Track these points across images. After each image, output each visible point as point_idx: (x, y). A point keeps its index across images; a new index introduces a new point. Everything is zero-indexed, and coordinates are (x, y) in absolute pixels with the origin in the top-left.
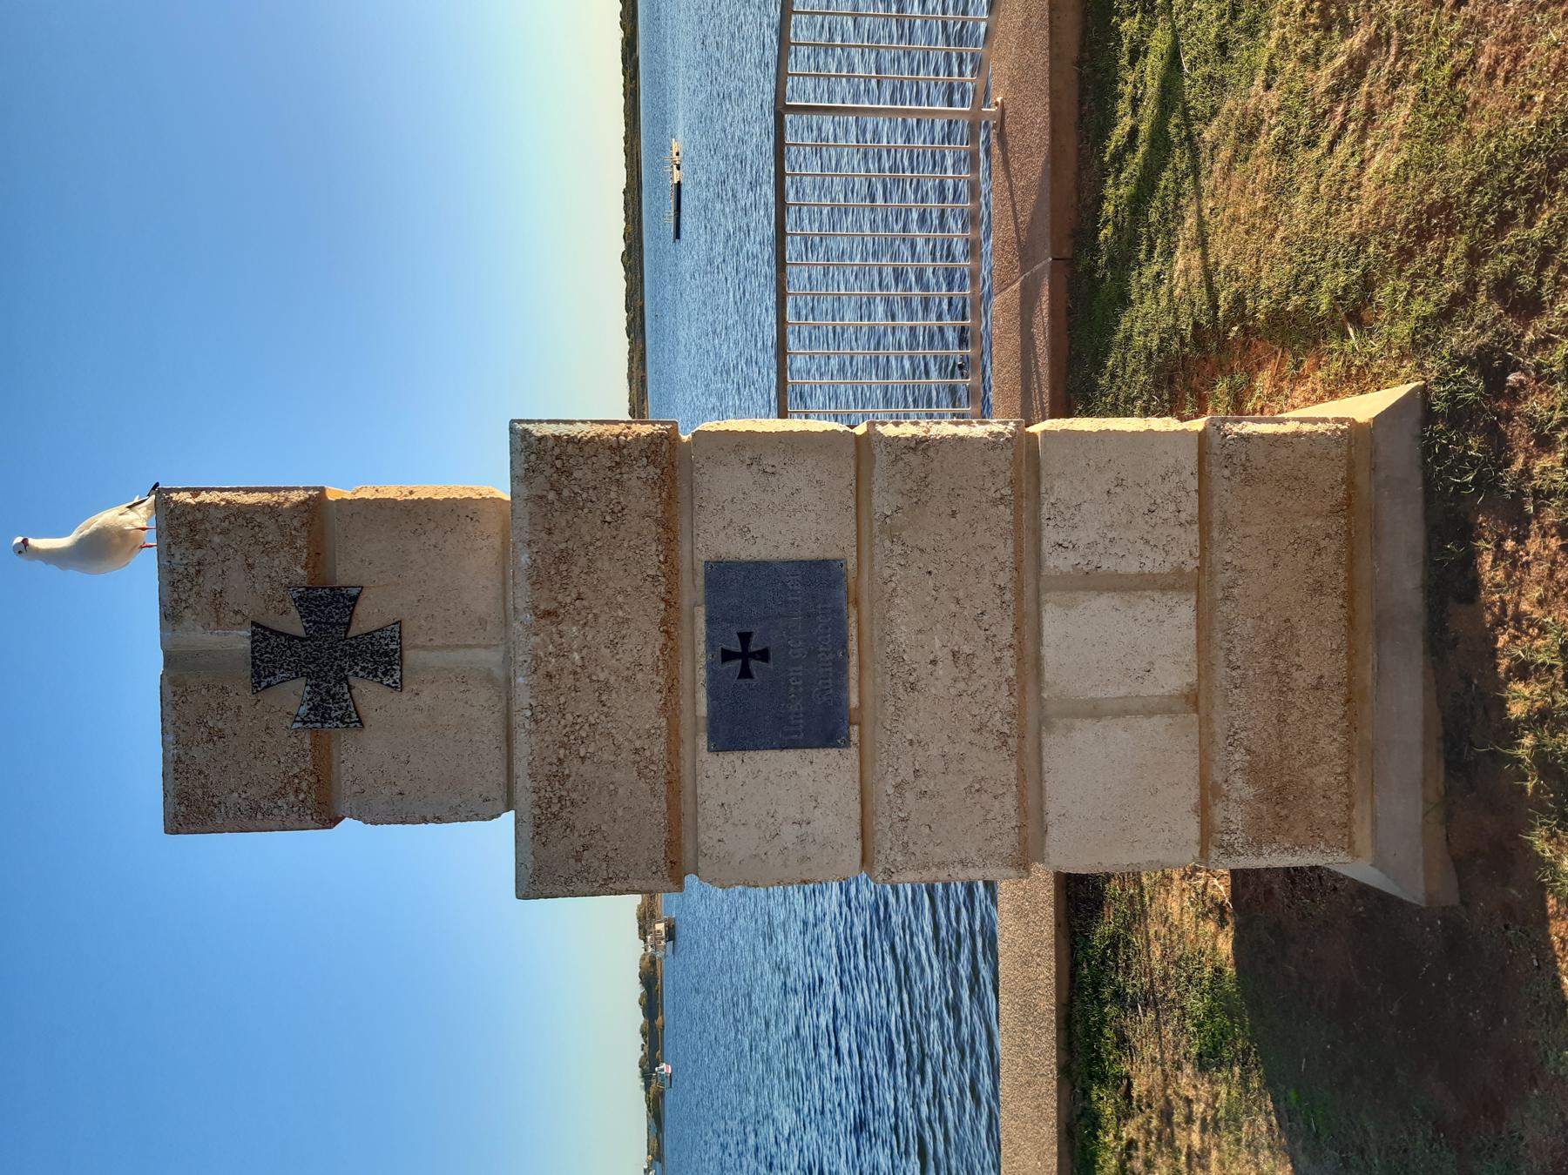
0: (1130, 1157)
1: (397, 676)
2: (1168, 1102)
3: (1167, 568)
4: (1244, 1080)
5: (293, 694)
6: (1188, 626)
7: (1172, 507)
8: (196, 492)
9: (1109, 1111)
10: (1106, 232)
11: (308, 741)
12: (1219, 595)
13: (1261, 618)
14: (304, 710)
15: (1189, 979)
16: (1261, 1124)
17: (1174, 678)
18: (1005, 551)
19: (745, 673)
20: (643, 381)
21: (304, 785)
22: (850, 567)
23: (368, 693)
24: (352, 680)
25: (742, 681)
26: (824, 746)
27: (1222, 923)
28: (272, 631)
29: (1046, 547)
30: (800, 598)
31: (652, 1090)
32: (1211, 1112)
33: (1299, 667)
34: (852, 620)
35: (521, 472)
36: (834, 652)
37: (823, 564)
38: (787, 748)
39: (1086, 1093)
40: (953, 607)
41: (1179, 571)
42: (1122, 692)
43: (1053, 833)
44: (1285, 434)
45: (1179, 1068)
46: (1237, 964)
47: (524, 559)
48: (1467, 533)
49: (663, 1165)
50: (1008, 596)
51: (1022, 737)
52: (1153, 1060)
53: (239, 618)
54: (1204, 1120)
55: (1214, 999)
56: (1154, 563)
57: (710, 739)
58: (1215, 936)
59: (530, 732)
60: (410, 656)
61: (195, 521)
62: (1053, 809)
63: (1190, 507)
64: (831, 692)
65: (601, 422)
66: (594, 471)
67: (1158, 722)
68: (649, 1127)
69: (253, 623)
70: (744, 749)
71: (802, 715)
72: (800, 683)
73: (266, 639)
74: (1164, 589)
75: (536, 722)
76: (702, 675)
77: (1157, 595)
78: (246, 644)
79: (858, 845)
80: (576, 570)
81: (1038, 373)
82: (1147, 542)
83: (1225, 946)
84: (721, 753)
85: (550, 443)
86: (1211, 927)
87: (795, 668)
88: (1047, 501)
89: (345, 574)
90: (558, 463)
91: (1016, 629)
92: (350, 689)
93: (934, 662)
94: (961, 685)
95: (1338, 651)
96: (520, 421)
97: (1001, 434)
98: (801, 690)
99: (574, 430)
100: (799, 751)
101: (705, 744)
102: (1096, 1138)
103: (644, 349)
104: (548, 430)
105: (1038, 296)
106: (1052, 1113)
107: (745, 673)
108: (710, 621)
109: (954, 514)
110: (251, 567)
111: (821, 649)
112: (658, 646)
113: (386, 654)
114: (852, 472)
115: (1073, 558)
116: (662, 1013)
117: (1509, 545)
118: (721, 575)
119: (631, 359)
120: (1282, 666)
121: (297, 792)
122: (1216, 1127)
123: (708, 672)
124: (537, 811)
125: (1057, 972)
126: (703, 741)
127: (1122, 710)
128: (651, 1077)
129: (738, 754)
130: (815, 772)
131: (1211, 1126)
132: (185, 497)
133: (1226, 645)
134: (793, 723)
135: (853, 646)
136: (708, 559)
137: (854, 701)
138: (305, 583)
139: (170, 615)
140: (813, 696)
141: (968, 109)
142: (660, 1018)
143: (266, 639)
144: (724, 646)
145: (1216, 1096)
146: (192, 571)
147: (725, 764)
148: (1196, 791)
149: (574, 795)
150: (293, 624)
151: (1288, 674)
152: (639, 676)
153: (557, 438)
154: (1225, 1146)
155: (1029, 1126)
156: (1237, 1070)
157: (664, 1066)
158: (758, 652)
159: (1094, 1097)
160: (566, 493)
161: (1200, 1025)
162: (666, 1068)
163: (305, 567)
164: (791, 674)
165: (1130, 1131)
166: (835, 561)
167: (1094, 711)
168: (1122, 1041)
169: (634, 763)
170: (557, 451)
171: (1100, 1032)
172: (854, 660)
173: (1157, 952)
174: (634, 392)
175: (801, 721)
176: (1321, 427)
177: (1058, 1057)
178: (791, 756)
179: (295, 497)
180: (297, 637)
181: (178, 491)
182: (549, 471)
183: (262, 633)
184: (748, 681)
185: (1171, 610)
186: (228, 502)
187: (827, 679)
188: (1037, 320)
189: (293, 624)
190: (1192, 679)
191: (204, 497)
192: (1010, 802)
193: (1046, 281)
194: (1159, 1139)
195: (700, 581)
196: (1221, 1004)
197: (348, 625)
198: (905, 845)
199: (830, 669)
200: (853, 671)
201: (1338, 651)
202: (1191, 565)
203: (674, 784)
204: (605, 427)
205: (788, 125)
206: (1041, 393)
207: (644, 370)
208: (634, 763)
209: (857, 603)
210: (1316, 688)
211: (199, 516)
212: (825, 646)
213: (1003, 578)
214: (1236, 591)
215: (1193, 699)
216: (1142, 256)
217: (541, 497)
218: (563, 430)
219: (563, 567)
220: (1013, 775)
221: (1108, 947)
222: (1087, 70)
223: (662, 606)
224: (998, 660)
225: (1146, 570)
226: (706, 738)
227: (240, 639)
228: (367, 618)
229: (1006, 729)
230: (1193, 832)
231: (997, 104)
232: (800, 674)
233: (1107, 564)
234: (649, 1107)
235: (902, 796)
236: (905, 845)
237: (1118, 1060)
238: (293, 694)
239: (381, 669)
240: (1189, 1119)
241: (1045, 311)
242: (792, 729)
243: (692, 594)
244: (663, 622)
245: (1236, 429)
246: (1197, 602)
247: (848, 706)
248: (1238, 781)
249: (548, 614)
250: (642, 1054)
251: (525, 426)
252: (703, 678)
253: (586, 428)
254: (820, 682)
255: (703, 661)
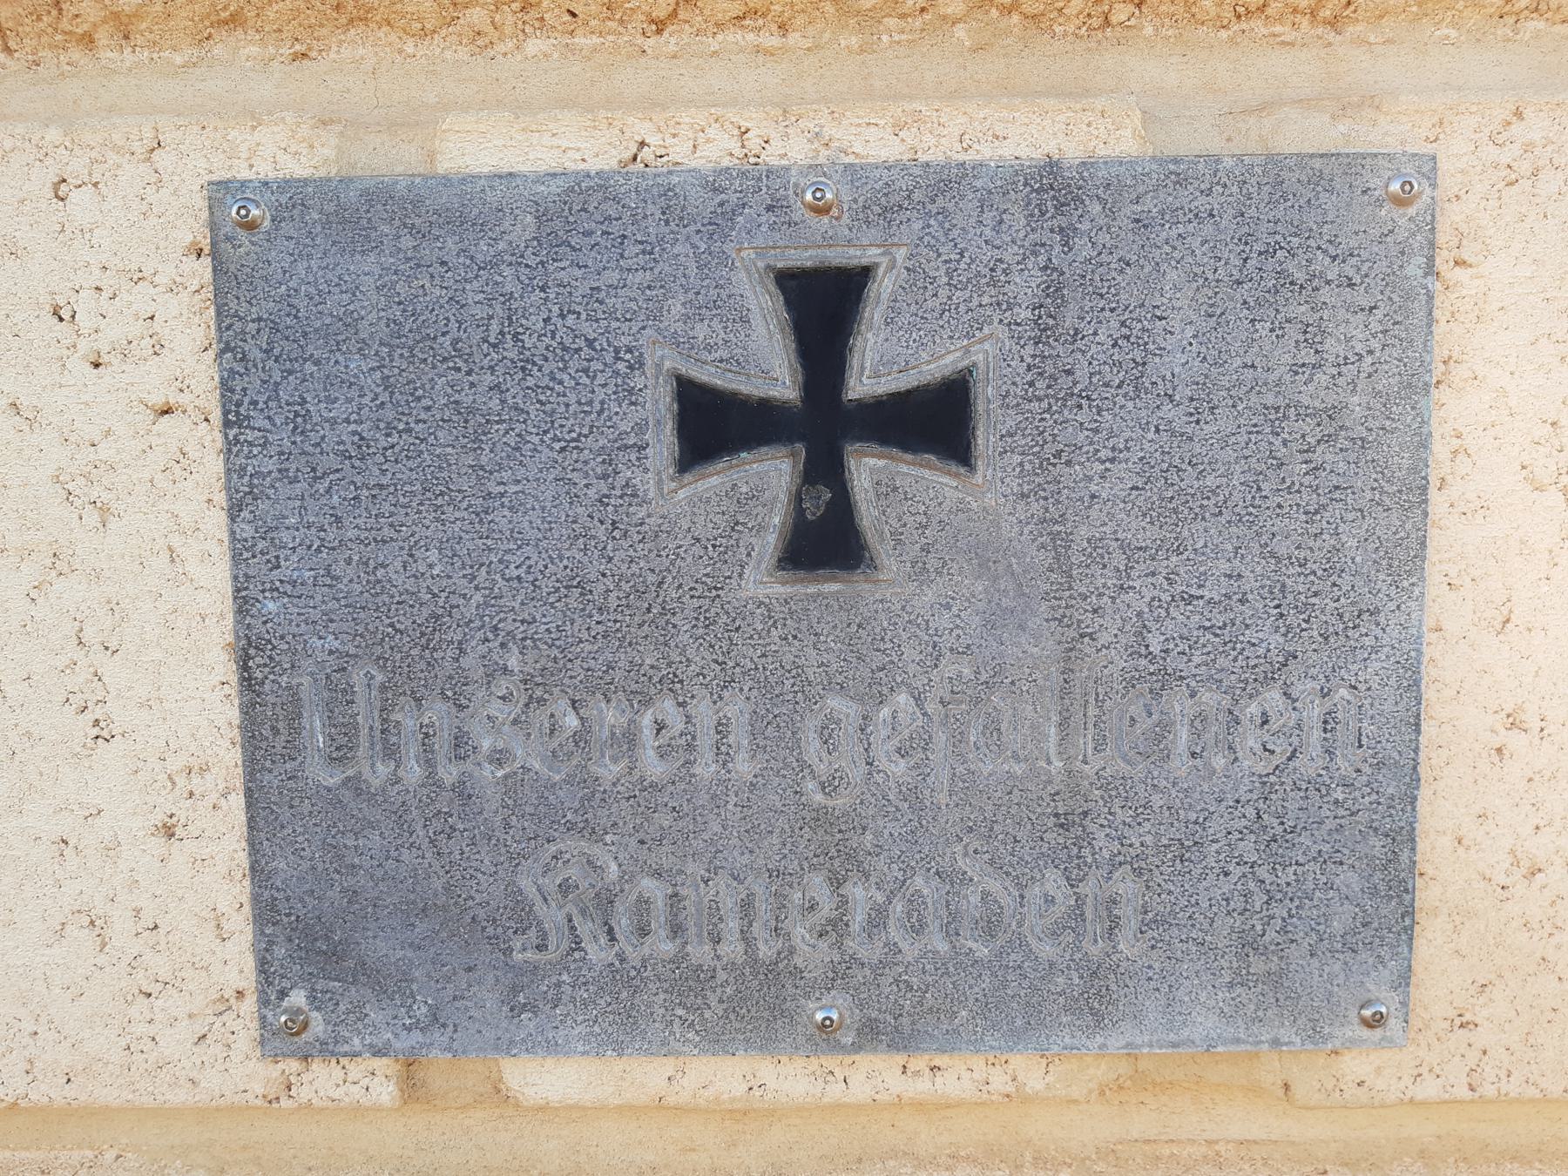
22: (1354, 1065)
25: (660, 404)
26: (266, 912)
30: (1180, 765)
36: (837, 976)
38: (248, 682)
64: (597, 953)
70: (232, 420)
71: (449, 773)
72: (653, 766)
84: (204, 268)
87: (739, 736)
98: (609, 770)
100: (229, 758)
101: (265, 170)
111: (857, 892)
123: (714, 183)
130: (111, 849)
134: (407, 720)
136: (1448, 181)
140: (571, 845)
144: (883, 287)
147: (139, 299)
158: (843, 506)
164: (704, 711)
166: (1404, 980)
175: (414, 772)
184: (663, 443)
187: (676, 930)
199: (732, 948)
205: (812, 589)
212: (877, 919)
222: (257, 566)
226: (298, 168)
232: (706, 769)
242: (364, 713)
247: (507, 1047)
252: (679, 152)
254: (648, 884)
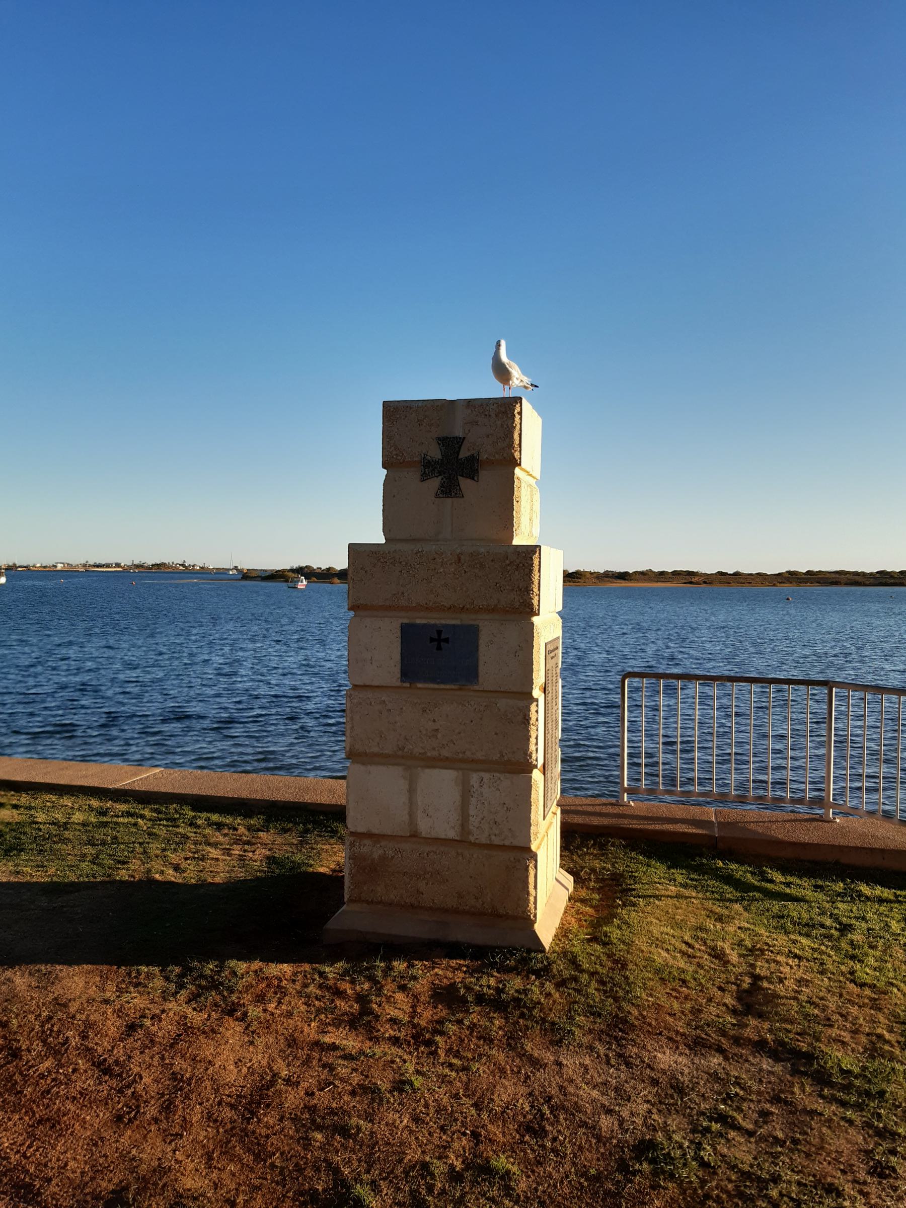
0: (230, 829)
1: (441, 495)
2: (254, 844)
3: (471, 827)
4: (260, 871)
5: (435, 453)
6: (446, 835)
7: (497, 832)
8: (520, 413)
9: (252, 822)
10: (720, 864)
11: (417, 459)
12: (459, 851)
13: (449, 868)
14: (429, 458)
15: (310, 856)
16: (241, 874)
17: (424, 826)
18: (480, 755)
19: (432, 640)
20: (836, 583)
21: (399, 458)
23: (435, 483)
24: (440, 478)
27: (334, 871)
28: (461, 445)
29: (482, 774)
31: (290, 574)
32: (248, 858)
33: (427, 884)
34: (453, 687)
35: (518, 550)
37: (476, 676)
39: (260, 813)
40: (457, 731)
41: (470, 833)
42: (419, 803)
43: (362, 768)
44: (528, 887)
45: (269, 850)
46: (313, 872)
47: (482, 550)
48: (473, 958)
49: (240, 580)
50: (461, 755)
51: (403, 757)
52: (275, 841)
53: (467, 432)
54: (245, 856)
55: (299, 864)
56: (474, 822)
57: (406, 624)
58: (328, 867)
59: (412, 551)
60: (449, 500)
61: (507, 414)
62: (373, 769)
63: (497, 841)
65: (539, 583)
66: (517, 580)
67: (406, 818)
68: (266, 571)
69: (464, 438)
73: (458, 443)
74: (462, 825)
75: (416, 553)
76: (432, 622)
77: (460, 822)
78: (457, 434)
79: (362, 684)
80: (477, 571)
81: (651, 824)
82: (483, 819)
83: (322, 870)
85: (530, 562)
86: (333, 866)
88: (502, 776)
89: (484, 474)
90: (521, 565)
91: (447, 758)
92: (437, 477)
93: (434, 721)
94: (424, 732)
95: (434, 903)
96: (540, 550)
97: (531, 757)
99: (536, 572)
102: (240, 816)
103: (865, 585)
104: (536, 562)
105: (702, 828)
106: (254, 796)
107: (432, 640)
108: (454, 626)
109: (496, 734)
110: (488, 436)
112: (445, 604)
113: (450, 491)
114: (515, 690)
115: (476, 785)
116: (342, 583)
117: (465, 969)
118: (473, 632)
119: (856, 574)
120: (428, 876)
121: (397, 455)
122: (241, 860)
124: (381, 553)
125: (323, 804)
126: (406, 621)
127: (411, 802)
128: (298, 573)
129: (400, 635)
131: (242, 858)
132: (517, 409)
133: (438, 852)
135: (442, 686)
137: (420, 685)
138: (480, 458)
139: (470, 403)
141: (831, 800)
142: (339, 581)
143: (458, 443)
145: (255, 861)
146: (487, 413)
148: (377, 832)
149: (387, 568)
150: (464, 454)
151: (424, 879)
152: (433, 596)
153: (532, 565)
154: (232, 862)
155: (248, 786)
156: (266, 869)
157: (305, 582)
159: (259, 816)
160: (509, 568)
161: (288, 858)
162: (303, 583)
163: (487, 458)
165: (242, 830)
167: (412, 791)
168: (285, 831)
169: (398, 592)
170: (526, 565)
171: (292, 822)
172: (436, 686)
173: (328, 847)
174: (828, 576)
176: (532, 905)
177: (281, 801)
178: (398, 657)
179: (516, 455)
180: (458, 455)
181: (521, 406)
182: (518, 561)
183: (460, 441)
185: (453, 828)
186: (515, 427)
188: (684, 826)
189: (464, 454)
190: (424, 835)
191: (517, 417)
192: (375, 750)
193: (704, 832)
194: (237, 839)
195: (472, 623)
196: (296, 866)
197: (462, 476)
198: (360, 703)
200: (432, 686)
201: (434, 903)
202: (472, 839)
203: (389, 608)
204: (537, 585)
206: (639, 825)
207: (846, 584)
208: (398, 592)
209: (460, 689)
210: (418, 891)
211: (509, 416)
213: (468, 754)
214: (460, 858)
215: (414, 835)
216: (692, 876)
217: (507, 558)
218: (536, 568)
219: (478, 566)
220: (386, 752)
221: (332, 828)
223: (461, 606)
224: (434, 749)
225: (471, 818)
227: (459, 433)
228: (465, 483)
229: (406, 750)
230: (361, 829)
231: (834, 818)
233: (473, 801)
234: (279, 571)
235: (380, 703)
236: (360, 703)
237: (276, 828)
238: (435, 453)
239: (444, 489)
240: (245, 851)
241: (686, 830)
243: (466, 619)
244: (454, 606)
245: (531, 865)
246: (456, 840)
248: (380, 852)
249: (459, 559)
250: (315, 568)
251: (538, 552)
253: (537, 577)
255: (438, 622)
